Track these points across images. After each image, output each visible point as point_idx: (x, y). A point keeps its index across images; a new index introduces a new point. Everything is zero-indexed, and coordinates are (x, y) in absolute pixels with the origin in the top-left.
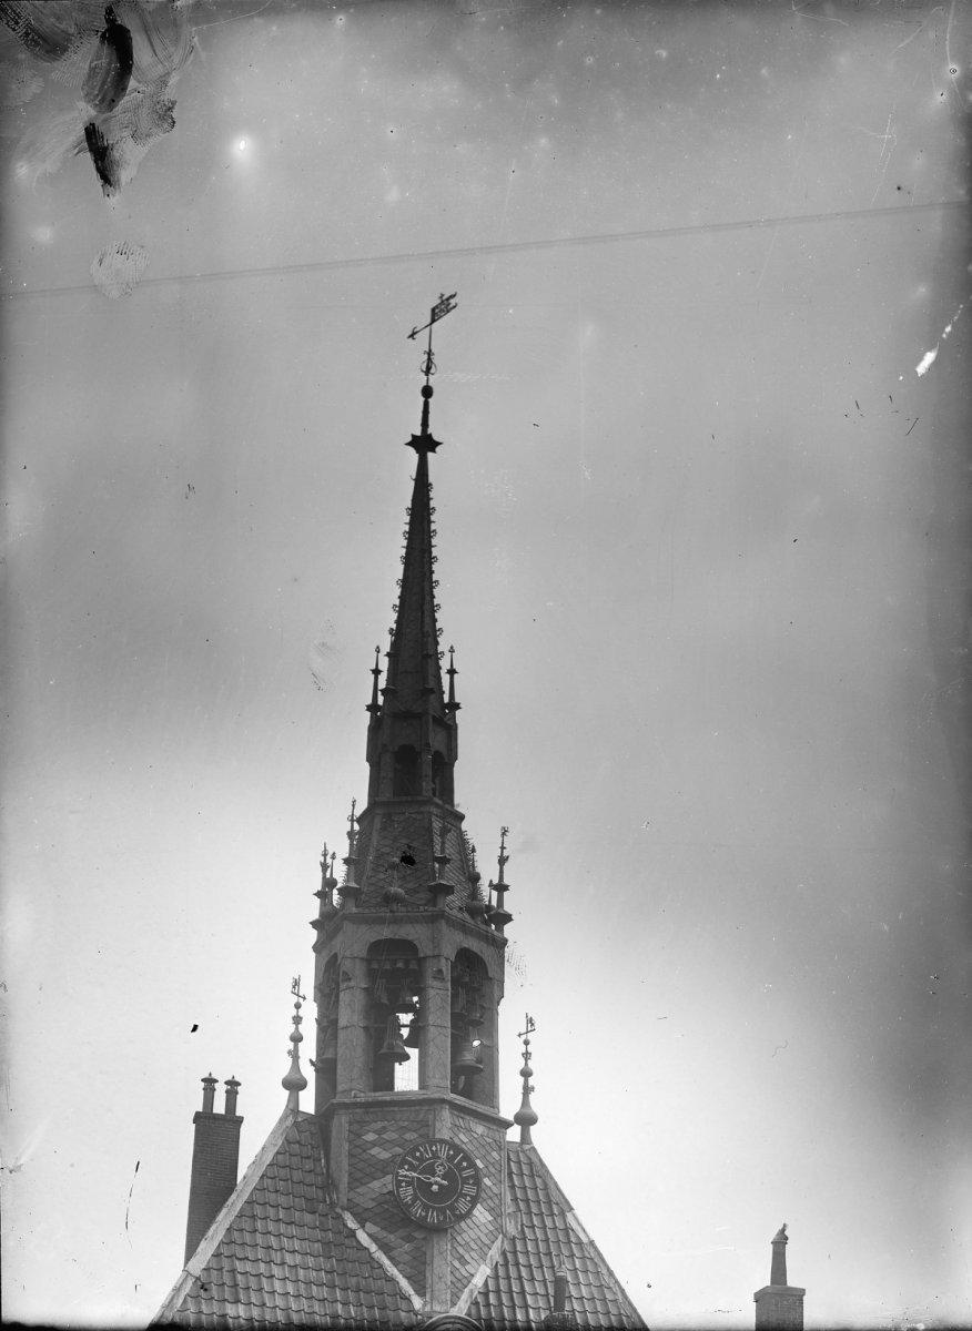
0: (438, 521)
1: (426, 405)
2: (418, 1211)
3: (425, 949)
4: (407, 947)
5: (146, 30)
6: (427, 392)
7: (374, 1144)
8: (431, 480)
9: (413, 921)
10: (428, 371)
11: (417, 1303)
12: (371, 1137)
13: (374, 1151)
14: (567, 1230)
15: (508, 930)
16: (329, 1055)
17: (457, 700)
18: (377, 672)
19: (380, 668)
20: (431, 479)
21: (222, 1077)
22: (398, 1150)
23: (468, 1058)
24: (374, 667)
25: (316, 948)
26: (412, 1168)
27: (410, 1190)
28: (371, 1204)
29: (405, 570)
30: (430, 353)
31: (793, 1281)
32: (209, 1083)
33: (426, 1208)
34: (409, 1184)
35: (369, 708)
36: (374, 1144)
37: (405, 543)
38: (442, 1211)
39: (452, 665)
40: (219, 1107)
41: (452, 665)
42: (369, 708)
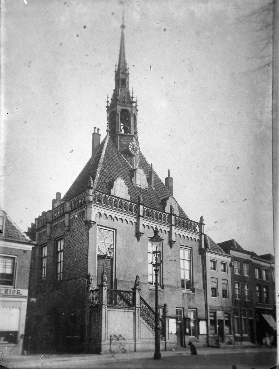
0: (126, 50)
2: (132, 152)
3: (130, 111)
4: (127, 111)
7: (123, 141)
11: (131, 167)
12: (123, 140)
13: (123, 143)
16: (89, 281)
18: (108, 102)
19: (109, 101)
20: (251, 251)
21: (97, 128)
22: (127, 143)
23: (135, 125)
24: (107, 101)
25: (107, 111)
26: (131, 145)
27: (131, 149)
29: (92, 157)
32: (95, 128)
33: (133, 152)
34: (131, 148)
36: (123, 141)
37: (41, 215)
38: (135, 153)
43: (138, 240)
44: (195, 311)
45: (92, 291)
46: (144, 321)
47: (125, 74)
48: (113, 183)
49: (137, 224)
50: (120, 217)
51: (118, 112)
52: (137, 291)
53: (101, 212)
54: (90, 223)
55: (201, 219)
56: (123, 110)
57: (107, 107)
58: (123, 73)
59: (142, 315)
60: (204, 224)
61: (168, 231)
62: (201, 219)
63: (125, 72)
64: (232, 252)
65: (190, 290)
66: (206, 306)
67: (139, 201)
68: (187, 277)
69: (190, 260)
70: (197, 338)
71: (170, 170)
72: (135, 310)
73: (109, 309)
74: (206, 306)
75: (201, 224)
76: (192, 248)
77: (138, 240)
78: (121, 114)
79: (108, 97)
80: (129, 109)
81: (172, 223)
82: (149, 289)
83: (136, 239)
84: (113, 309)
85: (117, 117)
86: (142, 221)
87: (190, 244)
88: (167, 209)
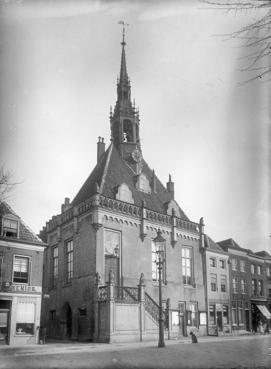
1: (124, 37)
2: (135, 159)
3: (132, 121)
4: (129, 121)
5: (185, 277)
6: (124, 36)
8: (125, 50)
9: (130, 117)
10: (124, 32)
14: (148, 168)
15: (140, 122)
17: (131, 85)
21: (102, 137)
28: (127, 158)
30: (124, 29)
31: (124, 42)
32: (100, 138)
33: (136, 159)
34: (134, 155)
35: (110, 118)
39: (124, 40)
41: (124, 40)
42: (110, 118)
43: (143, 240)
44: (196, 304)
45: (101, 288)
46: (149, 314)
49: (141, 226)
50: (195, 237)
51: (121, 122)
53: (107, 215)
54: (97, 226)
55: (201, 220)
58: (124, 86)
59: (147, 309)
60: (204, 225)
61: (170, 232)
62: (201, 220)
65: (191, 285)
66: (206, 300)
67: (143, 204)
69: (191, 258)
70: (197, 328)
71: (171, 175)
72: (141, 304)
73: (116, 304)
74: (206, 300)
75: (201, 225)
77: (143, 240)
79: (111, 109)
80: (131, 119)
82: (154, 285)
83: (140, 240)
84: (120, 304)
86: (146, 224)
87: (191, 243)
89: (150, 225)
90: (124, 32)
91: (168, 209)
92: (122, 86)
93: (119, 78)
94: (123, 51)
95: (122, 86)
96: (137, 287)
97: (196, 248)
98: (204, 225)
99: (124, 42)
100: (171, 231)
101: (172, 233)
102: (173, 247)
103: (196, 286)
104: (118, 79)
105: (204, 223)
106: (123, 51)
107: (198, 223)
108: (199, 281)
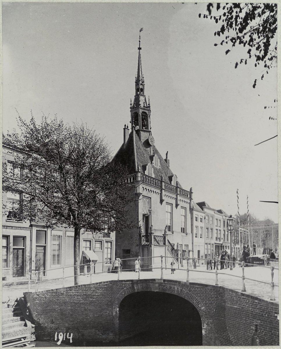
2: (150, 143)
4: (145, 113)
6: (140, 41)
30: (140, 36)
40: (173, 272)
41: (140, 46)
45: (143, 236)
47: (143, 85)
48: (172, 178)
49: (161, 194)
50: (153, 190)
51: (140, 114)
52: (166, 236)
54: (139, 195)
55: (191, 189)
56: (143, 112)
57: (131, 108)
58: (141, 84)
60: (192, 193)
61: (160, 193)
62: (191, 189)
63: (143, 84)
64: (205, 210)
67: (162, 179)
68: (169, 224)
72: (165, 247)
73: (154, 247)
75: (191, 193)
76: (186, 208)
78: (142, 115)
79: (131, 101)
80: (147, 112)
81: (162, 187)
84: (159, 247)
85: (139, 117)
86: (164, 192)
88: (173, 183)
89: (167, 194)
90: (140, 41)
91: (172, 181)
92: (140, 85)
93: (137, 77)
94: (139, 55)
95: (140, 85)
96: (163, 236)
97: (188, 209)
98: (192, 193)
99: (139, 50)
100: (160, 192)
101: (176, 199)
102: (177, 208)
103: (188, 234)
104: (136, 78)
105: (192, 191)
106: (139, 55)
107: (188, 191)
108: (189, 230)
